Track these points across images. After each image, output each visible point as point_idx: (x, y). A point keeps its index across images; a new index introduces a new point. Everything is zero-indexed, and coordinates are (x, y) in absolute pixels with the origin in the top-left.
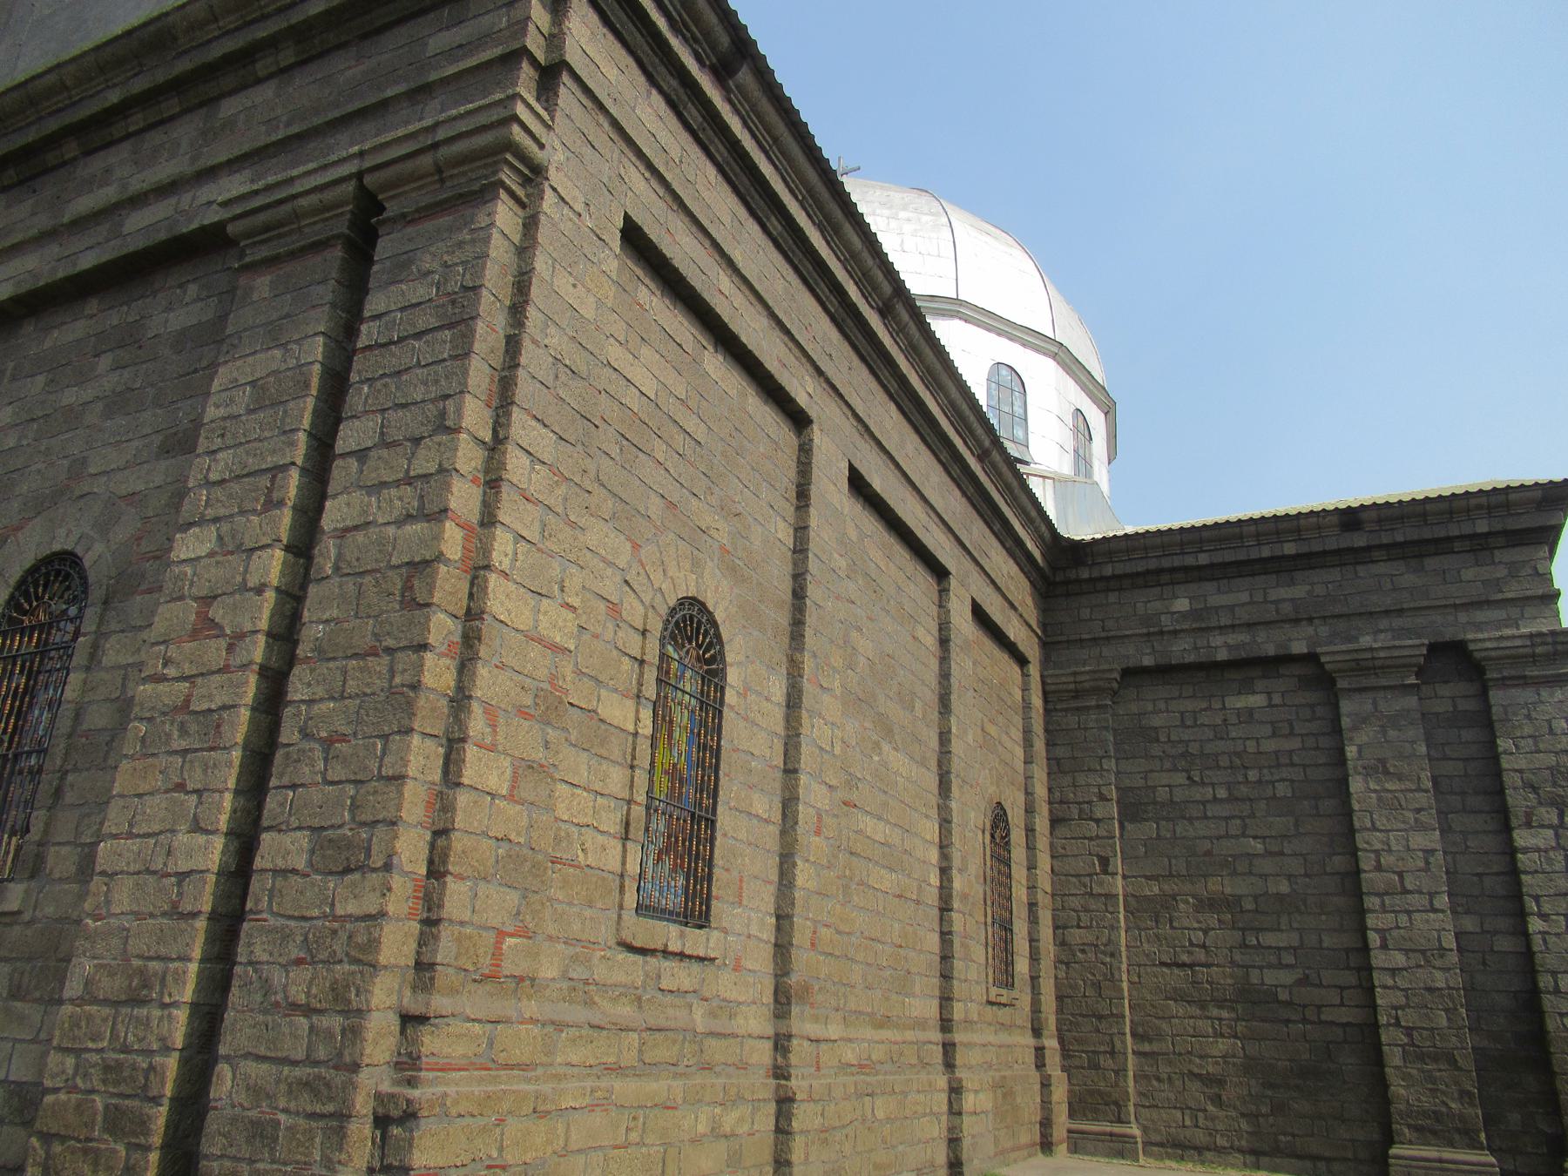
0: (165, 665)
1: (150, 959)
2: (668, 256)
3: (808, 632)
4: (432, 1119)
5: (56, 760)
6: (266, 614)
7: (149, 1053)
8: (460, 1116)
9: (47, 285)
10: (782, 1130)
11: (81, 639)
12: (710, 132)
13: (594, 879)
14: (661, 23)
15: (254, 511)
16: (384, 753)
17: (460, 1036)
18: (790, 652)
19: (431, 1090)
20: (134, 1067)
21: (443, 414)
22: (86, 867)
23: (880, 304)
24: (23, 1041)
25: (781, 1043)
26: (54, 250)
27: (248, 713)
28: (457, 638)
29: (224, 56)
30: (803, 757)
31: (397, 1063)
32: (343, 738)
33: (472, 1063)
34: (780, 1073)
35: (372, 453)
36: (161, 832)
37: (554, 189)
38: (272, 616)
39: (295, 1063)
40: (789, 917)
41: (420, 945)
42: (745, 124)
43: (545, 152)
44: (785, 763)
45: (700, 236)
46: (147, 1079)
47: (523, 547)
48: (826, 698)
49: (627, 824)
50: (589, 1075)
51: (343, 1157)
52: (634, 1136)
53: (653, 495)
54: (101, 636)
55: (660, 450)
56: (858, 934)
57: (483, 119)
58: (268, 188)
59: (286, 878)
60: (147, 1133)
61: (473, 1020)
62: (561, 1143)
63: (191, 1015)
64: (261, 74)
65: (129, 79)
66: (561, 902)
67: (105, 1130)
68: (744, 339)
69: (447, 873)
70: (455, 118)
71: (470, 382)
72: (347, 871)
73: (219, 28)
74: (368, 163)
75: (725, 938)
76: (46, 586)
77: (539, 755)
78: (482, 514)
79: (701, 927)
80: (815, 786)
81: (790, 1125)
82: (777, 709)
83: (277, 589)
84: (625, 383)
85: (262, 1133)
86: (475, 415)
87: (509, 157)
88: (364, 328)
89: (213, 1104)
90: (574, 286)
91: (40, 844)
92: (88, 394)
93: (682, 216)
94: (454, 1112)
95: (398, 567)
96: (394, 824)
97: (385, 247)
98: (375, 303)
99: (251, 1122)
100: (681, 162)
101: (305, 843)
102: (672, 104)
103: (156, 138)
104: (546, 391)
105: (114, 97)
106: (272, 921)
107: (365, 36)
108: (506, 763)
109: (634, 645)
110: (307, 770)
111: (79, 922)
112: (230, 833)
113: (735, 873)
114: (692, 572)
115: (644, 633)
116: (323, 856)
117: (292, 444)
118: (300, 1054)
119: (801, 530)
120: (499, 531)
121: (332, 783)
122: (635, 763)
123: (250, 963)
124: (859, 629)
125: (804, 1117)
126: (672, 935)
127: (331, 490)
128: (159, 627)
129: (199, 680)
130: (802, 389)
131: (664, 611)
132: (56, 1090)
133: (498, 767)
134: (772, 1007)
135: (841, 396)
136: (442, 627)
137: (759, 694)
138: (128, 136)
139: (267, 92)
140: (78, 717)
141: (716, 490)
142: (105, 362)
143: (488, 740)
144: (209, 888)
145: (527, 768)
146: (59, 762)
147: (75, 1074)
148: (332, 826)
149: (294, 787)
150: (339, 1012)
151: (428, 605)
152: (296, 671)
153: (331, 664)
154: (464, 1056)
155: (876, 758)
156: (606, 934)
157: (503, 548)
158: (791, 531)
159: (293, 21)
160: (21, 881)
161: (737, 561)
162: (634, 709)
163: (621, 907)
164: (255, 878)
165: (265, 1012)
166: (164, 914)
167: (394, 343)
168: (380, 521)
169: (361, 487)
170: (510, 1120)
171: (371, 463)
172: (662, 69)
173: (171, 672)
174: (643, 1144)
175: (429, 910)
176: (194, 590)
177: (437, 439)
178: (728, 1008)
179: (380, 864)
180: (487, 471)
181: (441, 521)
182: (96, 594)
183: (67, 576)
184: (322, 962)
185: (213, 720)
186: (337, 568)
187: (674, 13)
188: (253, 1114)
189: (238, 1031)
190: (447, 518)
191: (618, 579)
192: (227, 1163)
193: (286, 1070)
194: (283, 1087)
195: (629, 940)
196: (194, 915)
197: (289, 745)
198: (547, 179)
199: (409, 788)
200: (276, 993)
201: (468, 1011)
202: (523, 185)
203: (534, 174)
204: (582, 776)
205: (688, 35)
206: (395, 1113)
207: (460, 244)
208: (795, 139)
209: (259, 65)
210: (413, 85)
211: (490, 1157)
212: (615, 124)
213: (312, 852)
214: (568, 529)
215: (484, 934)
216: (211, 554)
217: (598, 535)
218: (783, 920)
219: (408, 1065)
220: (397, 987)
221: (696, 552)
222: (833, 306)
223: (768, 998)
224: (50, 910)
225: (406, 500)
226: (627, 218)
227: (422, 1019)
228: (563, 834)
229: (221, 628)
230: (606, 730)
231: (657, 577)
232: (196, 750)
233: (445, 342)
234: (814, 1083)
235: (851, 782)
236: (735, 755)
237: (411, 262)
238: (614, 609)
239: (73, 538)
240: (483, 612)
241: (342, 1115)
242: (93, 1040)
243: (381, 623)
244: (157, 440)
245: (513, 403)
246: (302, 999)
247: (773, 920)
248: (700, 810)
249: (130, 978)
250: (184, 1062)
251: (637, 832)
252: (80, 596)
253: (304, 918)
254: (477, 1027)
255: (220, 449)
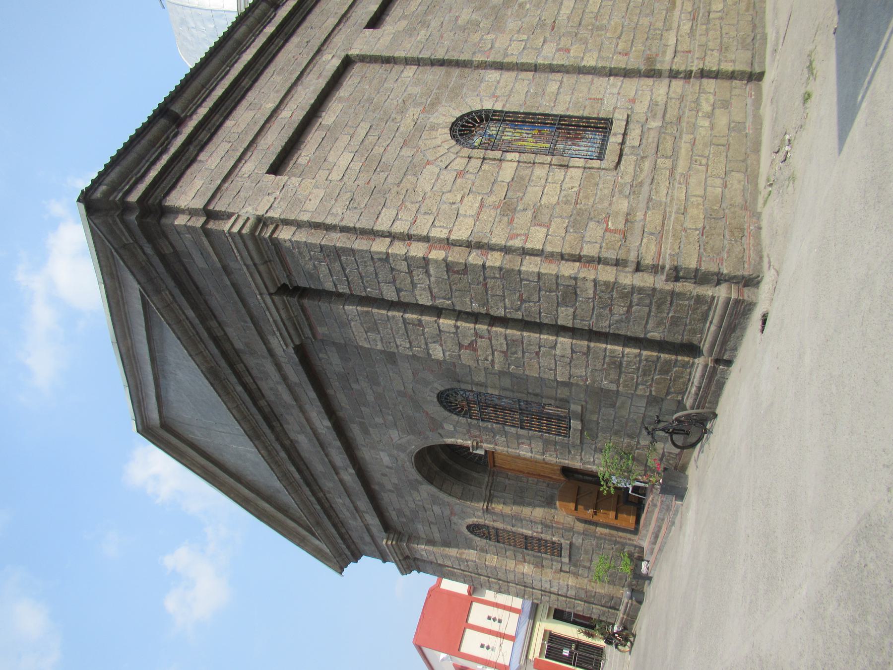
0: (487, 360)
1: (604, 362)
2: (281, 148)
3: (463, 57)
4: (679, 260)
5: (523, 396)
6: (467, 325)
7: (640, 361)
8: (679, 248)
9: (324, 408)
10: (716, 75)
11: (474, 389)
12: (210, 125)
13: (586, 183)
14: (165, 158)
15: (423, 330)
16: (529, 280)
17: (647, 247)
18: (473, 68)
19: (667, 260)
20: (645, 366)
21: (380, 259)
22: (567, 384)
23: (272, 10)
24: (631, 403)
25: (674, 75)
26: (307, 407)
27: (508, 330)
28: (479, 251)
29: (217, 348)
30: (528, 61)
31: (655, 273)
32: (521, 296)
33: (659, 242)
34: (688, 75)
35: (398, 286)
36: (555, 359)
37: (267, 212)
38: (468, 322)
39: (650, 311)
40: (611, 69)
41: (608, 265)
42: (200, 105)
43: (250, 217)
44: (531, 71)
45: (265, 130)
46: (650, 361)
47: (437, 223)
48: (497, 45)
49: (561, 166)
50: (673, 184)
51: (688, 293)
52: (704, 161)
53: (401, 154)
54: (473, 383)
55: (379, 150)
56: (623, 20)
57: (241, 246)
58: (279, 330)
59: (577, 315)
60: (671, 360)
61: (641, 242)
62: (699, 199)
63: (628, 347)
64: (222, 333)
65: (230, 383)
66: (595, 200)
67: (667, 374)
68: (312, 101)
69: (579, 255)
70: (242, 257)
71: (365, 249)
72: (576, 293)
73: (205, 351)
74: (264, 291)
75: (619, 108)
76: (451, 403)
77: (529, 214)
78: (424, 241)
79: (612, 123)
80: (544, 53)
81: (714, 71)
82: (503, 76)
83: (456, 321)
84: (349, 170)
85: (675, 322)
86: (380, 246)
87: (257, 234)
88: (341, 291)
89: (662, 339)
90: (310, 200)
91: (556, 400)
92: (369, 391)
93: (258, 140)
94: (677, 251)
95: (448, 276)
96: (558, 276)
97: (303, 283)
98: (329, 286)
99: (671, 325)
100: (230, 142)
101: (563, 309)
102: (202, 148)
103: (255, 372)
104: (363, 214)
105: (239, 388)
106: (594, 320)
107: (201, 293)
108: (533, 229)
109: (476, 163)
110: (533, 309)
111: (587, 386)
112: (557, 336)
113: (587, 103)
114: (437, 130)
115: (470, 158)
116: (569, 302)
117: (394, 317)
118: (647, 309)
119: (408, 61)
120: (431, 235)
121: (539, 299)
122: (532, 162)
123: (609, 327)
124: (457, 18)
125: (712, 64)
126: (614, 140)
127: (415, 302)
128: (472, 364)
129: (494, 348)
130: (330, 62)
131: (458, 147)
132: (651, 391)
133: (535, 233)
134: (655, 79)
135: (330, 35)
136: (475, 258)
137: (496, 88)
138: (254, 382)
139: (230, 331)
140: (505, 389)
141: (393, 116)
142: (355, 386)
143: (523, 238)
144: (579, 342)
145: (536, 220)
146: (524, 395)
147: (645, 385)
148: (557, 299)
149: (540, 313)
150: (632, 295)
151: (466, 264)
152: (492, 313)
153: (490, 300)
154: (655, 246)
155: (528, 6)
156: (610, 176)
157: (439, 233)
158: (408, 67)
159: (199, 322)
160: (570, 406)
161: (428, 102)
162: (507, 162)
163: (599, 168)
164: (576, 326)
165: (629, 321)
166: (587, 357)
167: (347, 279)
168: (428, 283)
169: (413, 290)
170: (685, 226)
171: (402, 286)
172: (187, 155)
173: (490, 358)
174: (708, 158)
175: (594, 261)
176: (456, 351)
177: (391, 262)
178: (653, 105)
179: (574, 282)
180: (404, 240)
181: (429, 259)
182: (455, 385)
183: (448, 395)
184: (611, 302)
185: (511, 343)
186: (448, 299)
187: (159, 151)
188: (667, 325)
189: (636, 331)
190: (427, 257)
191: (445, 172)
192: (685, 333)
193: (652, 314)
194: (659, 315)
195: (614, 164)
196: (588, 347)
197: (523, 315)
198: (263, 215)
199: (543, 271)
200: (622, 318)
201: (637, 244)
202: (267, 227)
203: (261, 222)
204: (539, 189)
205: (166, 142)
206: (674, 274)
207: (300, 253)
208: (199, 74)
209: (219, 335)
210: (224, 273)
211: (698, 235)
212: (225, 180)
213: (567, 306)
214: (426, 201)
215: (606, 237)
216: (441, 345)
217: (425, 182)
218: (612, 73)
219: (656, 269)
220: (624, 274)
221: (427, 128)
222: (280, 42)
223: (650, 81)
224: (582, 396)
225: (419, 273)
226: (268, 172)
227: (638, 263)
228: (564, 199)
229: (473, 341)
230: (517, 177)
231: (442, 150)
232: (523, 348)
233: (347, 259)
234: (696, 56)
235: (541, 24)
236: (528, 103)
237: (309, 273)
238: (460, 174)
239: (432, 394)
240: (468, 241)
241: (672, 294)
242: (634, 379)
243: (473, 282)
244: (389, 366)
245: (372, 229)
246: (625, 309)
247: (612, 78)
248: (555, 124)
249: (611, 368)
250: (646, 349)
251: (564, 160)
252: (455, 391)
253: (593, 309)
254: (645, 240)
255: (396, 344)
